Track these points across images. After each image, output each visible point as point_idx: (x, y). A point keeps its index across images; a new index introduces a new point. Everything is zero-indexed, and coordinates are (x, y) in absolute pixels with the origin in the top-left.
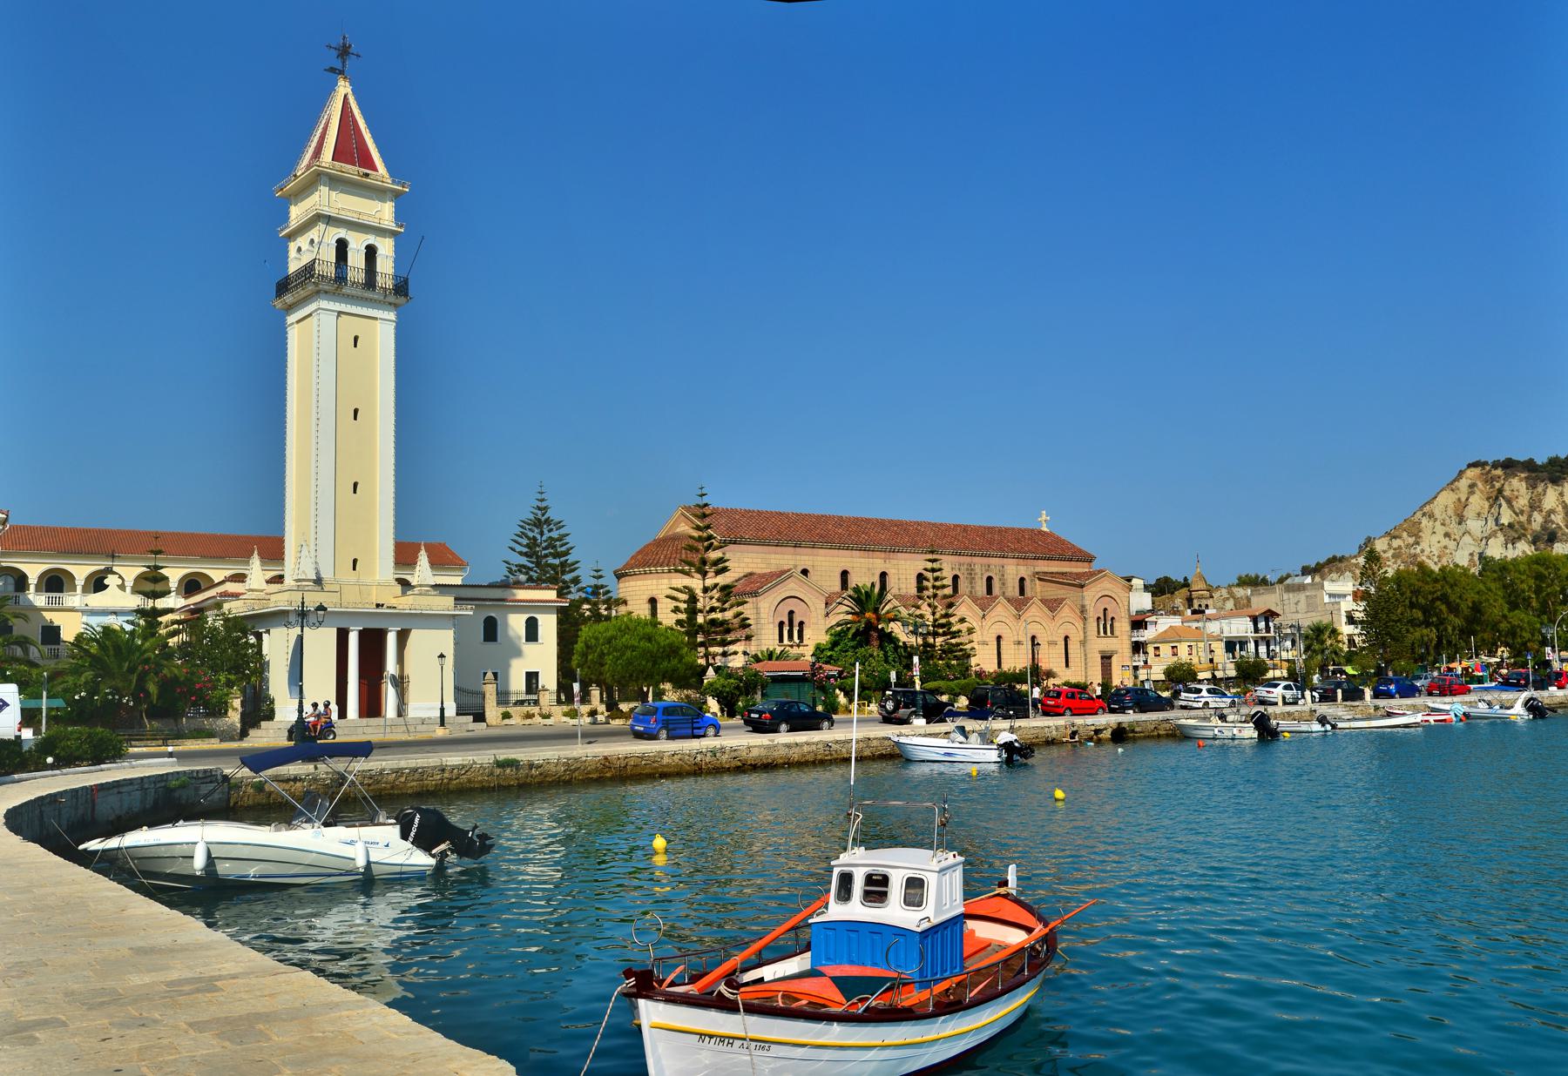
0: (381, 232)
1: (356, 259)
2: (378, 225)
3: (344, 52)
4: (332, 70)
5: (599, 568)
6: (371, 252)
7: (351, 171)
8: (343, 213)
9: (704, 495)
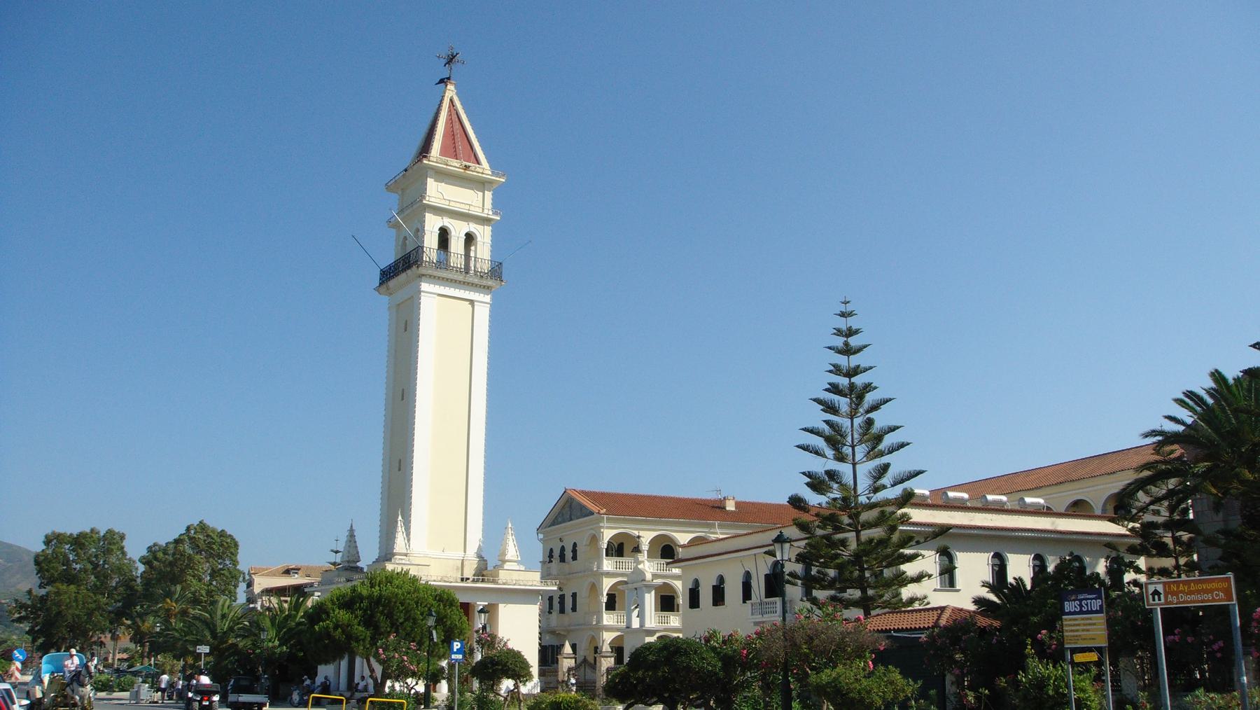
0: (484, 221)
1: (457, 245)
2: (467, 211)
3: (451, 59)
4: (442, 81)
5: (847, 300)
6: (470, 239)
7: (455, 165)
8: (452, 204)
9: (848, 302)
